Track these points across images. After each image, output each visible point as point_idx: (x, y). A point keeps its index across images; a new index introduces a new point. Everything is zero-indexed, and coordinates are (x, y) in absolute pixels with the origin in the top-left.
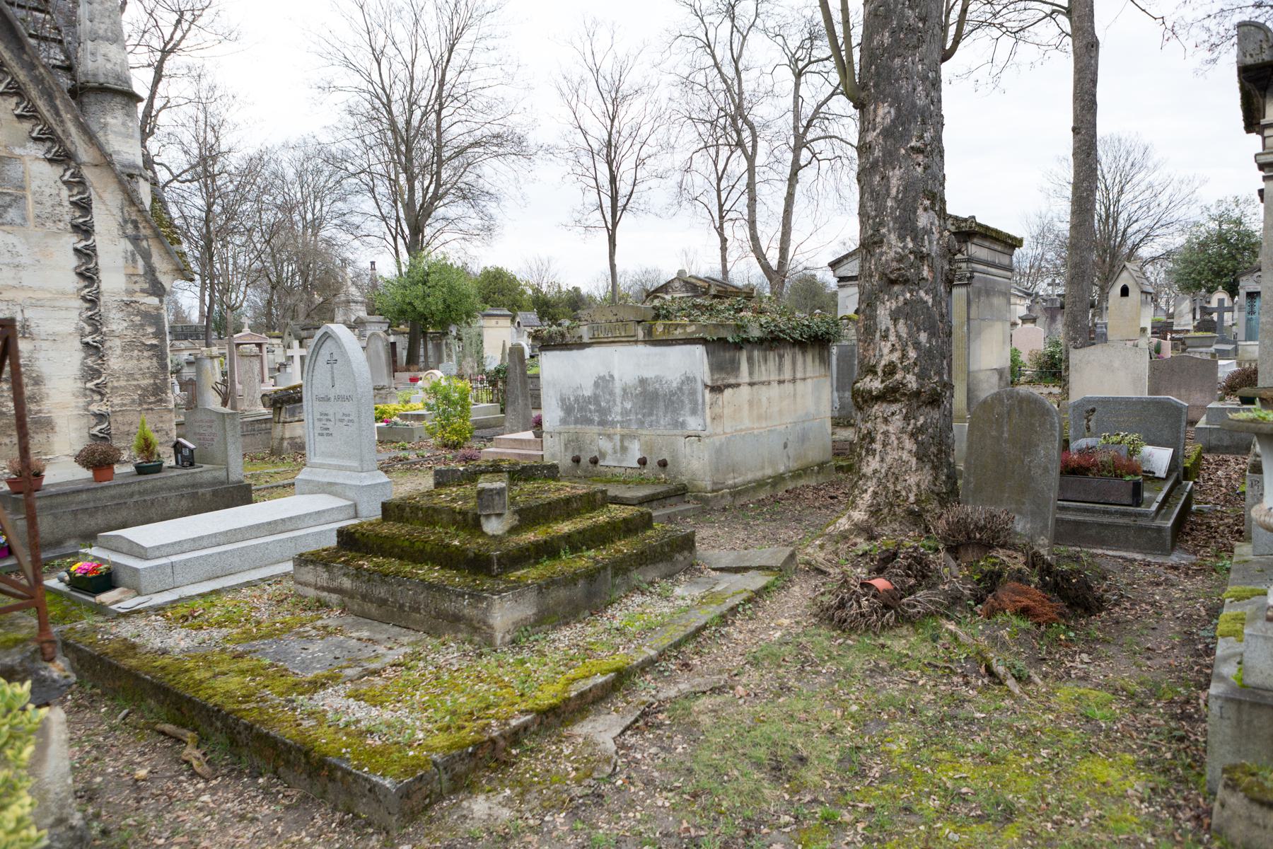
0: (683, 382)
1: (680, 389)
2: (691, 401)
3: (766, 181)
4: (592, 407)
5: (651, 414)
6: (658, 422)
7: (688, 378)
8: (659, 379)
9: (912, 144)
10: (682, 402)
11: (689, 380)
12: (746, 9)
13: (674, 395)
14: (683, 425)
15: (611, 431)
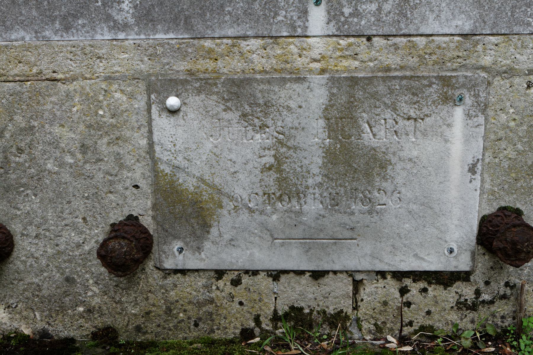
15: (257, 55)
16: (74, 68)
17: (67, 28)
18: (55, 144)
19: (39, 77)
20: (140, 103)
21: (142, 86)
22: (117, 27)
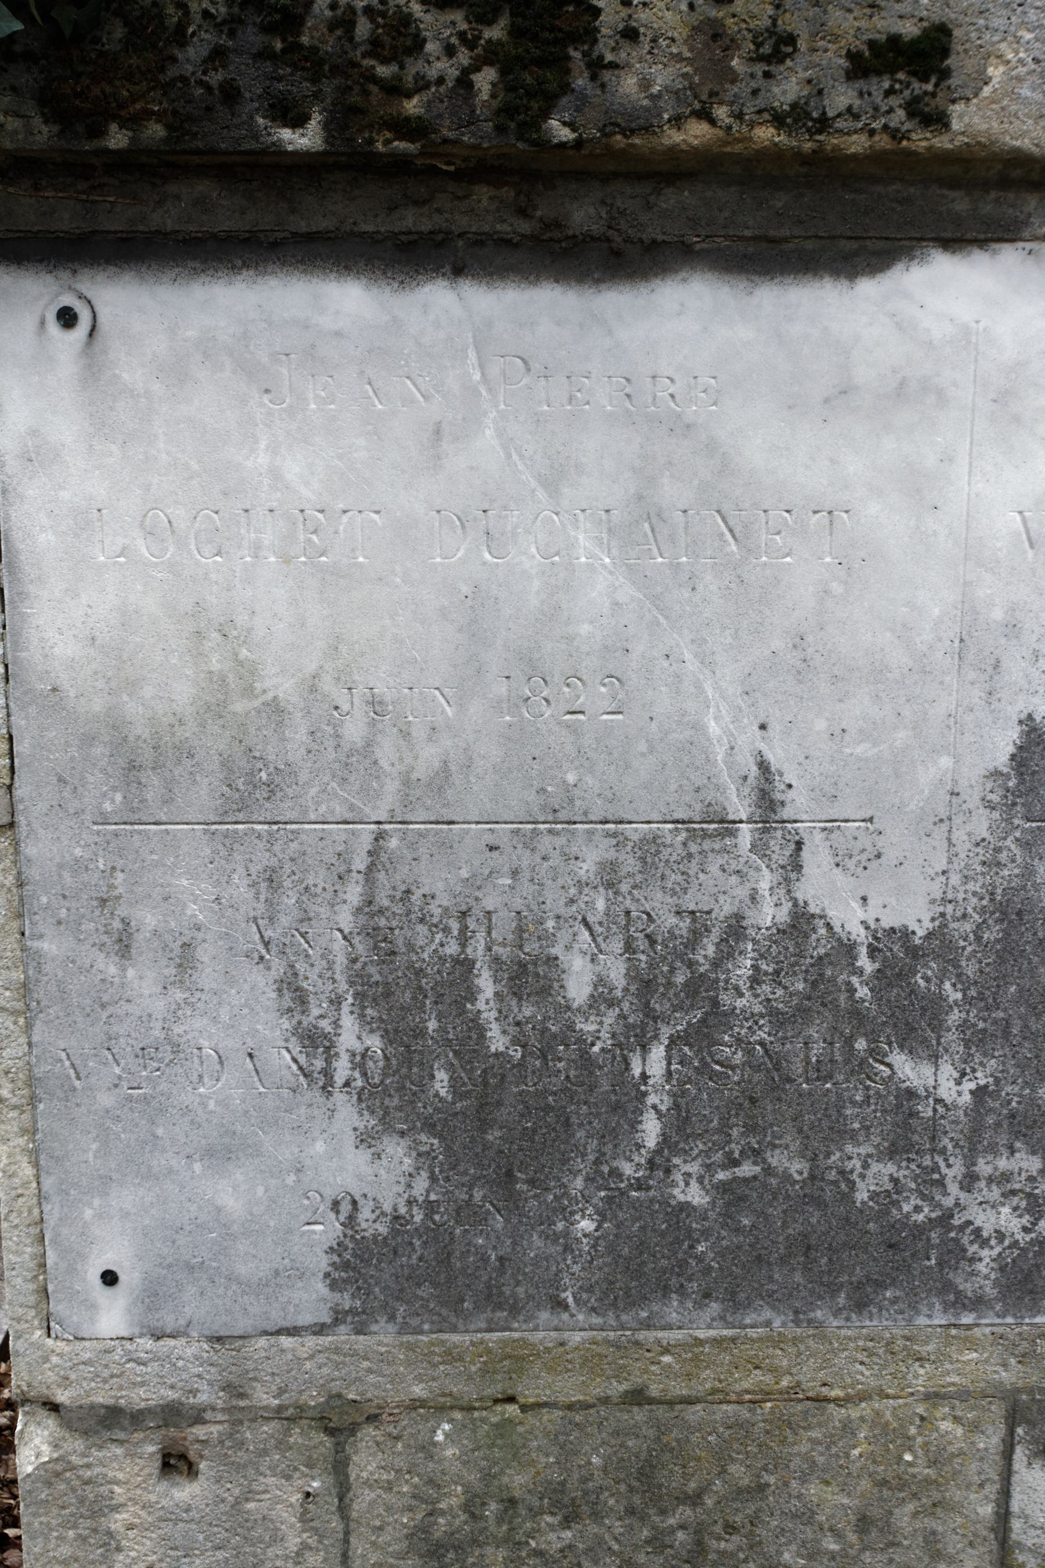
4: (943, 1081)
16: (866, 1376)
17: (860, 1305)
18: (807, 1516)
19: (792, 1394)
20: (991, 1440)
21: (998, 1409)
22: (960, 1302)
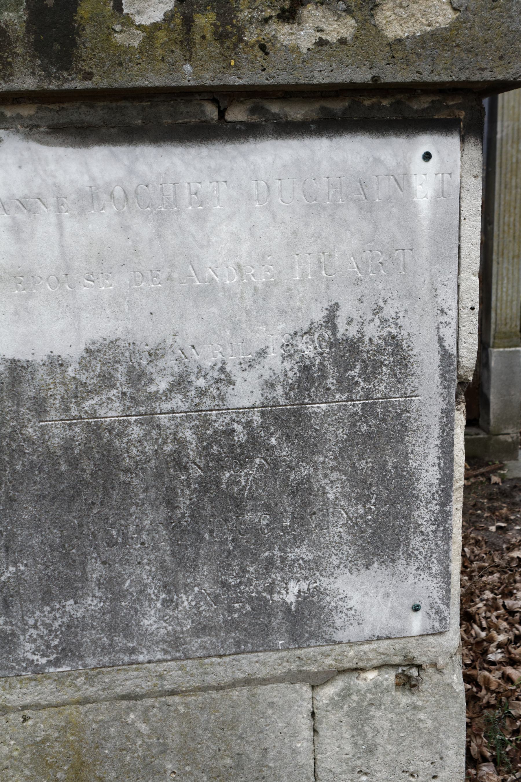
0: (307, 378)
1: (288, 418)
2: (360, 488)
3: (464, 326)
5: (63, 584)
6: (120, 624)
7: (347, 352)
8: (114, 366)
9: (198, 283)
10: (304, 493)
11: (350, 361)
12: (520, 651)
13: (240, 456)
14: (307, 620)
